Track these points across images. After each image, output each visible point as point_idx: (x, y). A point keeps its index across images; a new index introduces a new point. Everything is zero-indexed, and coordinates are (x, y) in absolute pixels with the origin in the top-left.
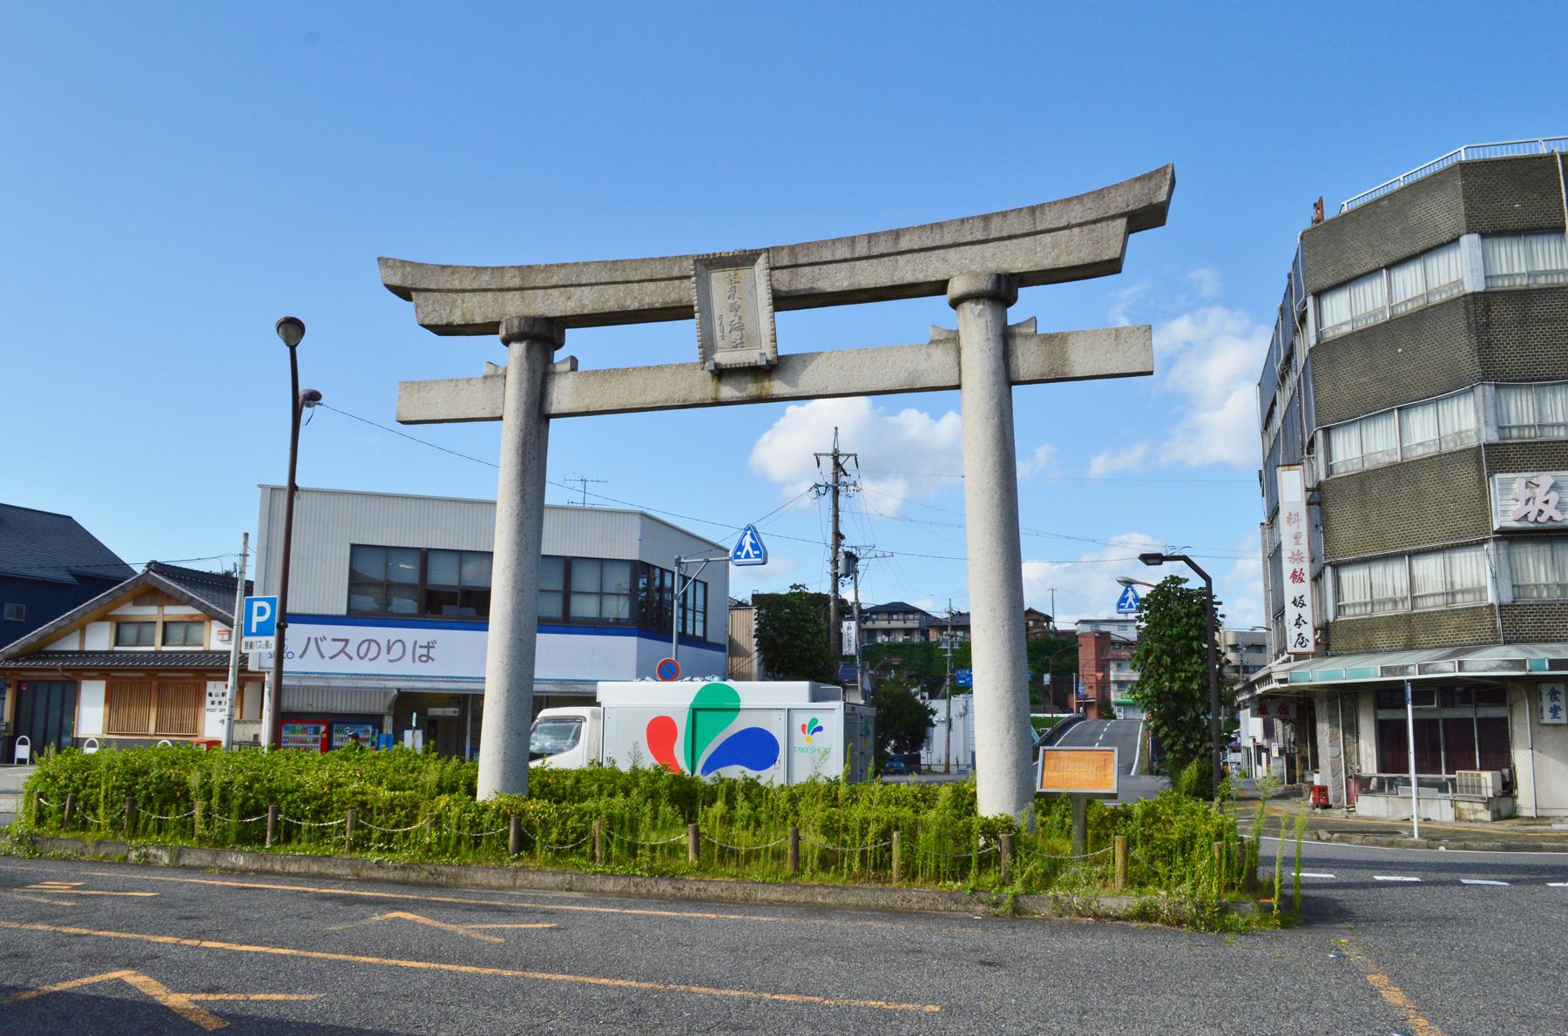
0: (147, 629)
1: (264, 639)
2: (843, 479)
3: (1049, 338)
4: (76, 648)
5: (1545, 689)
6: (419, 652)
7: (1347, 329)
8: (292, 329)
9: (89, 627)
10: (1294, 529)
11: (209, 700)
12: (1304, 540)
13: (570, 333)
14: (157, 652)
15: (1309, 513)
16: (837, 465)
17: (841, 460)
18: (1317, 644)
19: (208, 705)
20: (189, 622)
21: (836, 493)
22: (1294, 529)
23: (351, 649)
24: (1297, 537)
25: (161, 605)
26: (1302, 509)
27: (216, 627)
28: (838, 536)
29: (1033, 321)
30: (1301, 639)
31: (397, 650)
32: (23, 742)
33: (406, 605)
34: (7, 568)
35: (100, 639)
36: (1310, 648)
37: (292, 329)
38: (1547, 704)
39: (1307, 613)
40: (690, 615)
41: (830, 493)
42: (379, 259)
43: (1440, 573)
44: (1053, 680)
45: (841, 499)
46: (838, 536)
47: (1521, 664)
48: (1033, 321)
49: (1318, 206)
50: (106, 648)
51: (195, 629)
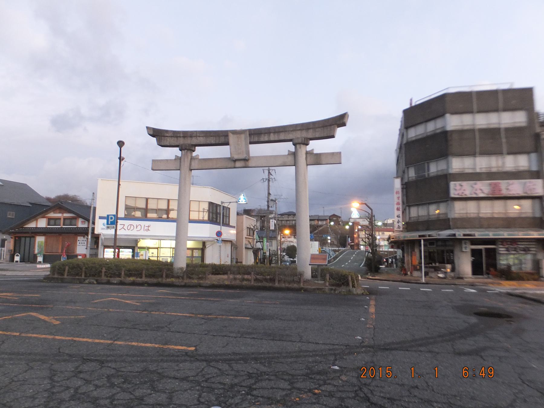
0: (57, 221)
1: (112, 226)
2: (271, 176)
3: (317, 154)
4: (34, 226)
5: (463, 242)
6: (146, 228)
7: (414, 139)
8: (121, 144)
9: (39, 220)
10: (397, 196)
11: (78, 242)
12: (400, 199)
13: (197, 148)
14: (62, 228)
15: (402, 191)
16: (269, 173)
17: (271, 171)
18: (403, 228)
19: (78, 244)
20: (71, 219)
21: (269, 181)
22: (397, 196)
23: (125, 227)
24: (398, 198)
25: (63, 213)
26: (400, 190)
27: (80, 220)
28: (269, 194)
29: (313, 150)
30: (399, 227)
31: (139, 228)
32: (17, 256)
33: (138, 214)
34: (2, 201)
35: (42, 223)
36: (401, 229)
37: (121, 144)
38: (464, 246)
39: (401, 219)
40: (225, 217)
41: (267, 181)
42: (147, 127)
43: (194, 253)
44: (80, 259)
45: (271, 183)
46: (269, 194)
47: (454, 235)
48: (313, 150)
49: (411, 100)
50: (45, 226)
51: (73, 221)
